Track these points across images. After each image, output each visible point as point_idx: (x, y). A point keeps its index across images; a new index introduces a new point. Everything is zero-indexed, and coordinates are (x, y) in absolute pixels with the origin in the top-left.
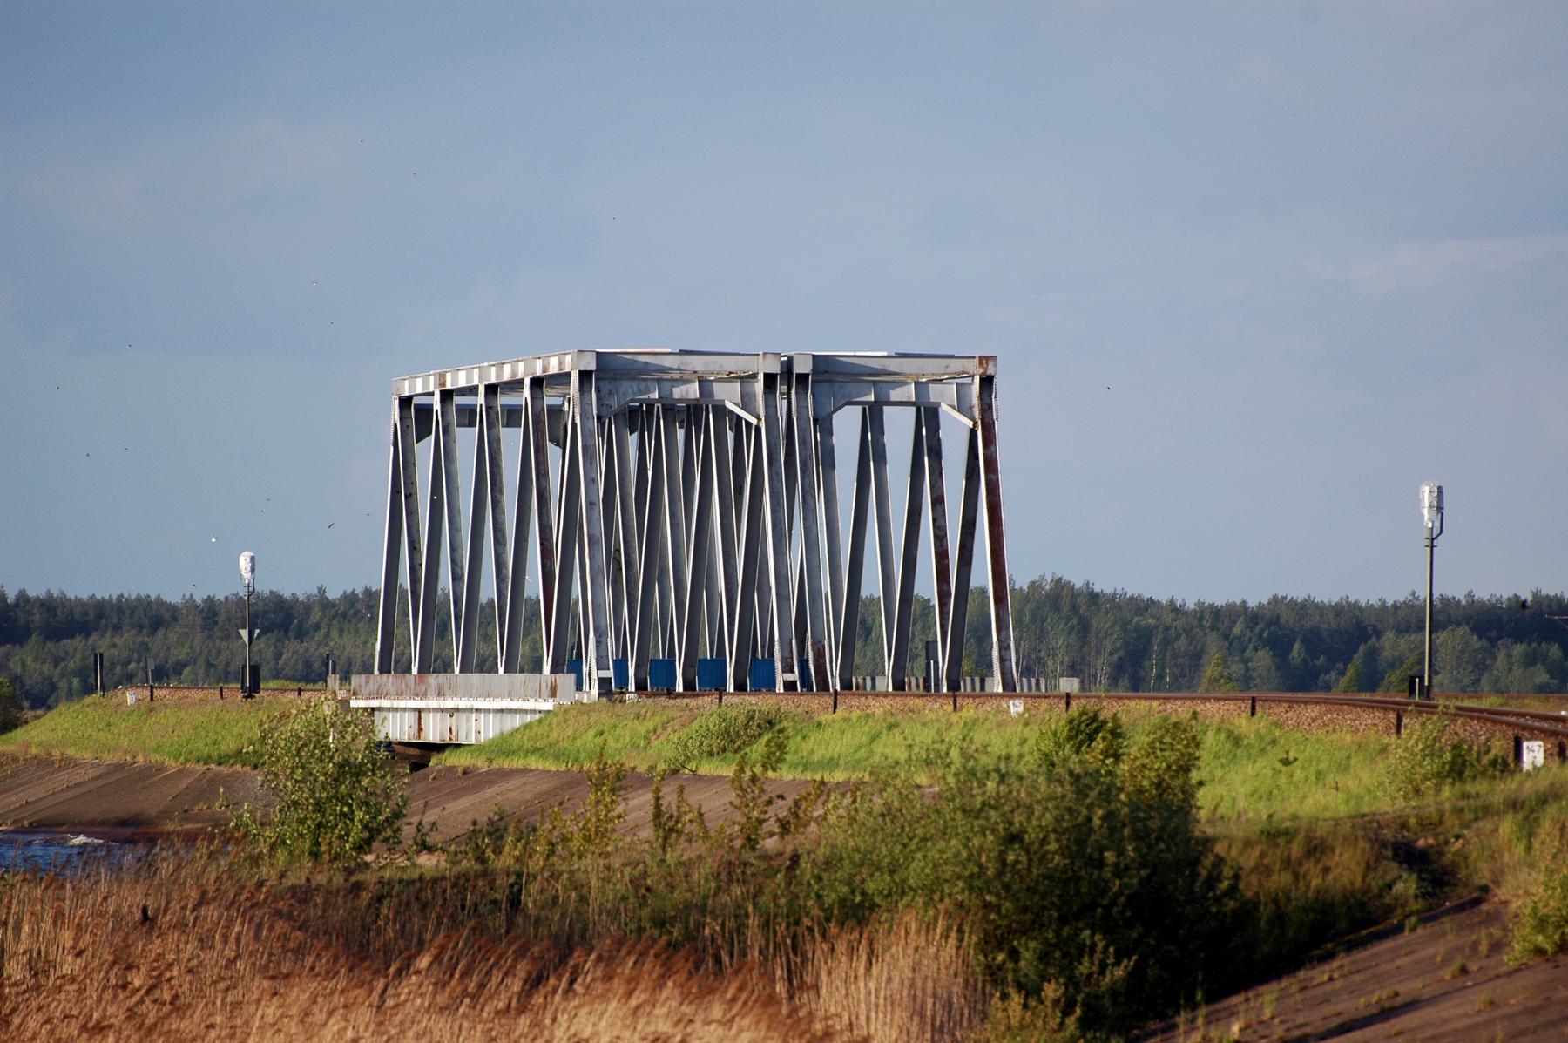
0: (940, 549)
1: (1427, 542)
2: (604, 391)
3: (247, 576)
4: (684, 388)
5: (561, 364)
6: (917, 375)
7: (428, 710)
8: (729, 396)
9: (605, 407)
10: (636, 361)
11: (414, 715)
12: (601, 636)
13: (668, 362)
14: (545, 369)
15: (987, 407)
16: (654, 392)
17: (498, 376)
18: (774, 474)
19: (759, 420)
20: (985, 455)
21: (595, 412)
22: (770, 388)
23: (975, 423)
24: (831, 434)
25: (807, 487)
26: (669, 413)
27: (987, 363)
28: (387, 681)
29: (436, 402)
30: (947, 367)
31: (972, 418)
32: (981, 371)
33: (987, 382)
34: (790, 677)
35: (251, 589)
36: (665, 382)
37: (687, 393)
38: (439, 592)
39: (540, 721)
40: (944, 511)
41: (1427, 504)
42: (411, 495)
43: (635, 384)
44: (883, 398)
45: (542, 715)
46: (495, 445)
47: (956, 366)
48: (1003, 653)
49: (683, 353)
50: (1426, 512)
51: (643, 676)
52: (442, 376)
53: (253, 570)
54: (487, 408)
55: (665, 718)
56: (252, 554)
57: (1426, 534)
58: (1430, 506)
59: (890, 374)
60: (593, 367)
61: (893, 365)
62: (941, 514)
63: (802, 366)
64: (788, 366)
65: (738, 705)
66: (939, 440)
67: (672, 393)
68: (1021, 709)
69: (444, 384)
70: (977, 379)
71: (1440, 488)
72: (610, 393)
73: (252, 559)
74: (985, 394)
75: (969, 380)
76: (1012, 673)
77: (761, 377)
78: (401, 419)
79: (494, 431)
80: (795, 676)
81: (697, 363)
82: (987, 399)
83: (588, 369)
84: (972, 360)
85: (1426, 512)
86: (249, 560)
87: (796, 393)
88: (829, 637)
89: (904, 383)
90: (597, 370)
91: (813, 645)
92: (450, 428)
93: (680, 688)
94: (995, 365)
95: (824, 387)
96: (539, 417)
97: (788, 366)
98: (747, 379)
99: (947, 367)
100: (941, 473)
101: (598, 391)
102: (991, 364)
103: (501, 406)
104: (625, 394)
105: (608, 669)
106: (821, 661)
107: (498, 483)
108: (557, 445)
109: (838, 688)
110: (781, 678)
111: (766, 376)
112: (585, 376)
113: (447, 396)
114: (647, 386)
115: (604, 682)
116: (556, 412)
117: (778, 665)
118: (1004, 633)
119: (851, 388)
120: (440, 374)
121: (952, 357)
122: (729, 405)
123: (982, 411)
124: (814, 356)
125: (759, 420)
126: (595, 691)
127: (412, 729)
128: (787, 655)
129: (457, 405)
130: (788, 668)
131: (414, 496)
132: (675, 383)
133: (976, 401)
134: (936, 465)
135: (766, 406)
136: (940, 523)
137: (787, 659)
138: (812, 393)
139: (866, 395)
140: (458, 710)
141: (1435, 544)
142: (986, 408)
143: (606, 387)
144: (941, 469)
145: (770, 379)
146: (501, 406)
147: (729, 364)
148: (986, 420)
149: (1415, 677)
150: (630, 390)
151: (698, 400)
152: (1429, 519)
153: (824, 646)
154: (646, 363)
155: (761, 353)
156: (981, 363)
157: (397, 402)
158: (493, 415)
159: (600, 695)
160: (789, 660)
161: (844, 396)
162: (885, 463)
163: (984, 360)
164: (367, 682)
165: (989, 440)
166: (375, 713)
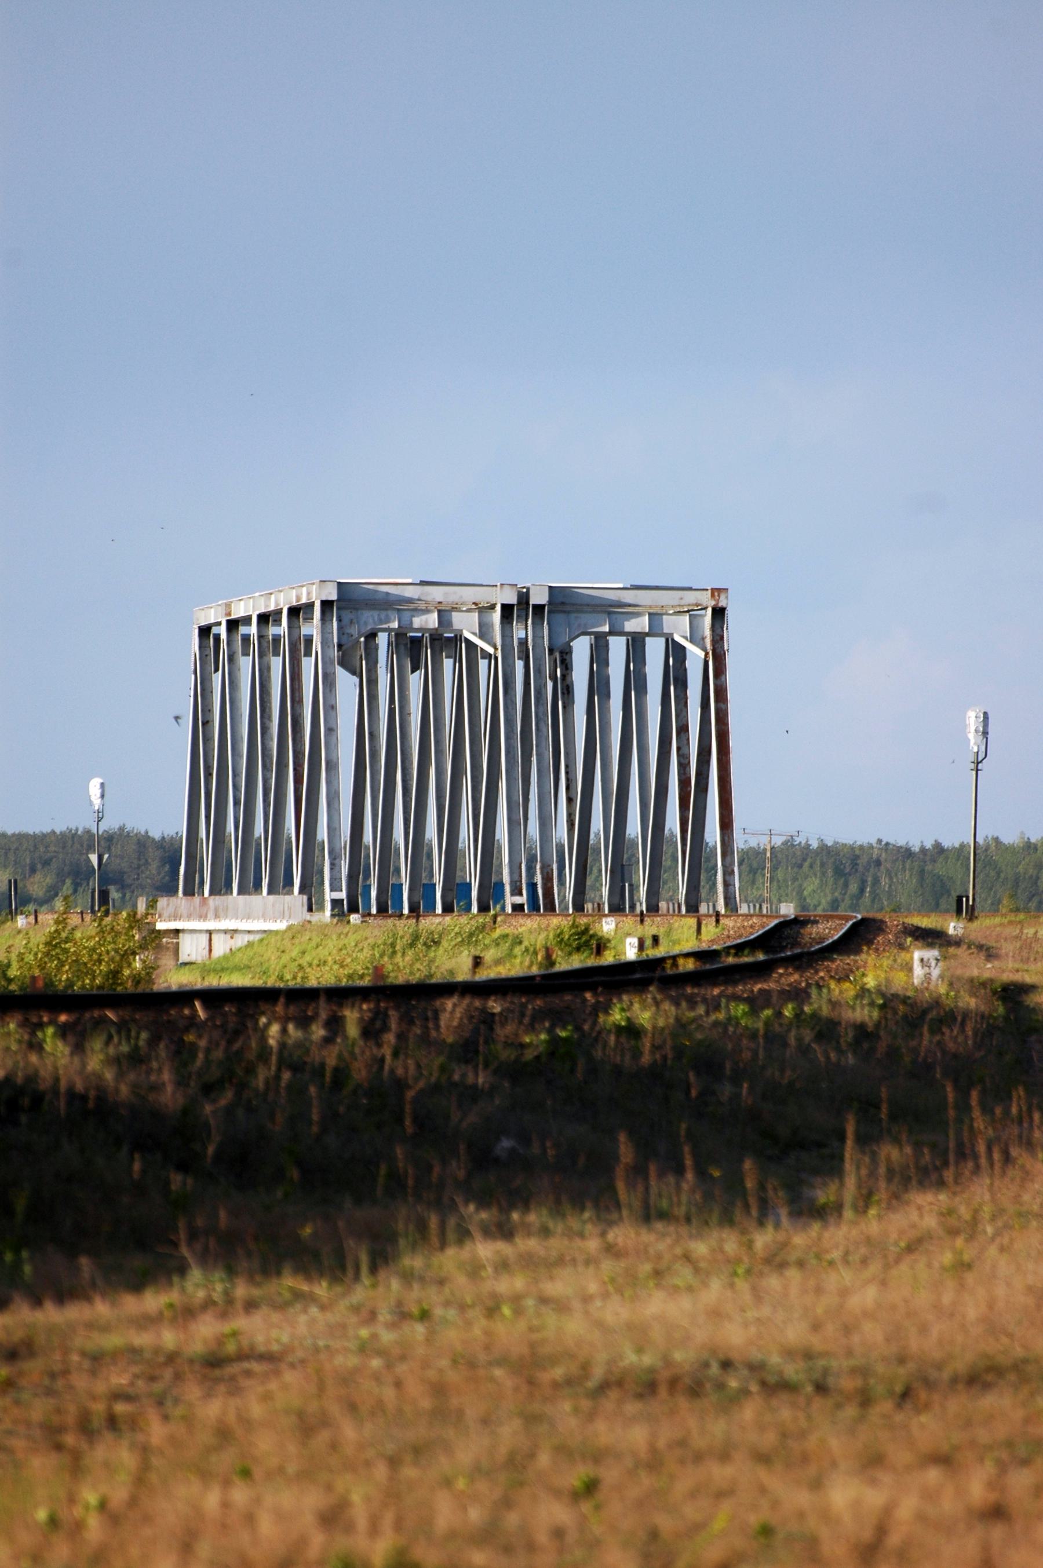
0: (683, 777)
1: (973, 766)
2: (346, 620)
3: (97, 802)
4: (424, 617)
5: (309, 594)
6: (650, 607)
7: (218, 931)
8: (466, 625)
9: (345, 636)
10: (376, 591)
11: (205, 938)
12: (335, 859)
13: (410, 592)
14: (298, 599)
15: (718, 638)
16: (394, 621)
17: (266, 606)
18: (509, 702)
19: (496, 649)
20: (715, 685)
21: (335, 640)
22: (507, 618)
23: (707, 654)
24: (607, 664)
25: (540, 714)
26: (436, 642)
27: (719, 596)
28: (181, 903)
29: (223, 631)
30: (681, 599)
31: (704, 649)
32: (713, 603)
33: (719, 613)
34: (518, 900)
35: (100, 815)
36: (406, 612)
37: (426, 622)
38: (666, 831)
39: (261, 940)
40: (688, 739)
41: (972, 728)
42: (208, 722)
43: (375, 613)
44: (617, 629)
45: (264, 935)
46: (266, 674)
47: (690, 598)
48: (727, 878)
49: (424, 583)
50: (971, 736)
51: (416, 899)
52: (228, 606)
53: (102, 796)
54: (596, 646)
55: (359, 937)
56: (102, 781)
57: (972, 758)
58: (976, 731)
59: (630, 605)
60: (334, 597)
61: (628, 597)
62: (686, 742)
63: (540, 597)
64: (524, 598)
65: (404, 927)
66: (685, 670)
67: (411, 623)
68: (613, 926)
69: (229, 614)
70: (709, 611)
71: (985, 714)
72: (351, 622)
73: (102, 785)
74: (717, 626)
75: (703, 612)
76: (735, 898)
77: (498, 608)
78: (200, 647)
79: (265, 659)
80: (522, 899)
81: (436, 594)
82: (719, 631)
83: (330, 599)
84: (705, 592)
85: (971, 736)
86: (98, 786)
87: (533, 623)
88: (345, 854)
89: (638, 615)
90: (338, 600)
91: (542, 868)
92: (236, 656)
93: (406, 911)
94: (727, 597)
95: (560, 618)
96: (296, 645)
97: (524, 598)
98: (485, 609)
99: (681, 599)
100: (686, 703)
101: (339, 620)
102: (723, 597)
103: (273, 635)
104: (366, 623)
105: (341, 891)
106: (549, 885)
107: (267, 710)
108: (354, 673)
109: (644, 909)
110: (510, 900)
111: (504, 606)
112: (326, 605)
113: (233, 625)
114: (387, 616)
115: (336, 903)
116: (277, 639)
117: (507, 889)
118: (728, 859)
119: (585, 618)
120: (226, 604)
121: (690, 589)
122: (467, 634)
123: (714, 642)
124: (550, 587)
125: (496, 649)
126: (328, 912)
127: (204, 951)
128: (516, 878)
129: (242, 635)
130: (517, 891)
131: (210, 723)
132: (414, 613)
133: (708, 632)
134: (682, 695)
135: (503, 636)
136: (684, 751)
137: (516, 882)
138: (548, 623)
139: (601, 625)
140: (235, 931)
141: (979, 768)
142: (718, 639)
143: (347, 616)
144: (686, 698)
145: (507, 610)
146: (273, 635)
147: (469, 595)
148: (718, 651)
149: (963, 897)
150: (371, 621)
151: (436, 629)
152: (975, 744)
153: (552, 870)
154: (387, 594)
155: (499, 584)
156: (713, 595)
157: (197, 631)
158: (265, 644)
159: (333, 916)
160: (518, 884)
161: (579, 625)
162: (646, 693)
163: (716, 592)
164: (168, 905)
165: (720, 670)
166: (181, 935)
